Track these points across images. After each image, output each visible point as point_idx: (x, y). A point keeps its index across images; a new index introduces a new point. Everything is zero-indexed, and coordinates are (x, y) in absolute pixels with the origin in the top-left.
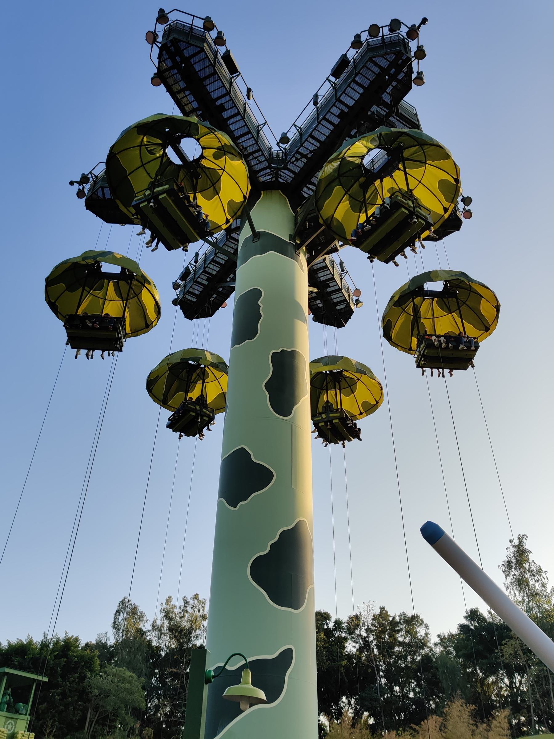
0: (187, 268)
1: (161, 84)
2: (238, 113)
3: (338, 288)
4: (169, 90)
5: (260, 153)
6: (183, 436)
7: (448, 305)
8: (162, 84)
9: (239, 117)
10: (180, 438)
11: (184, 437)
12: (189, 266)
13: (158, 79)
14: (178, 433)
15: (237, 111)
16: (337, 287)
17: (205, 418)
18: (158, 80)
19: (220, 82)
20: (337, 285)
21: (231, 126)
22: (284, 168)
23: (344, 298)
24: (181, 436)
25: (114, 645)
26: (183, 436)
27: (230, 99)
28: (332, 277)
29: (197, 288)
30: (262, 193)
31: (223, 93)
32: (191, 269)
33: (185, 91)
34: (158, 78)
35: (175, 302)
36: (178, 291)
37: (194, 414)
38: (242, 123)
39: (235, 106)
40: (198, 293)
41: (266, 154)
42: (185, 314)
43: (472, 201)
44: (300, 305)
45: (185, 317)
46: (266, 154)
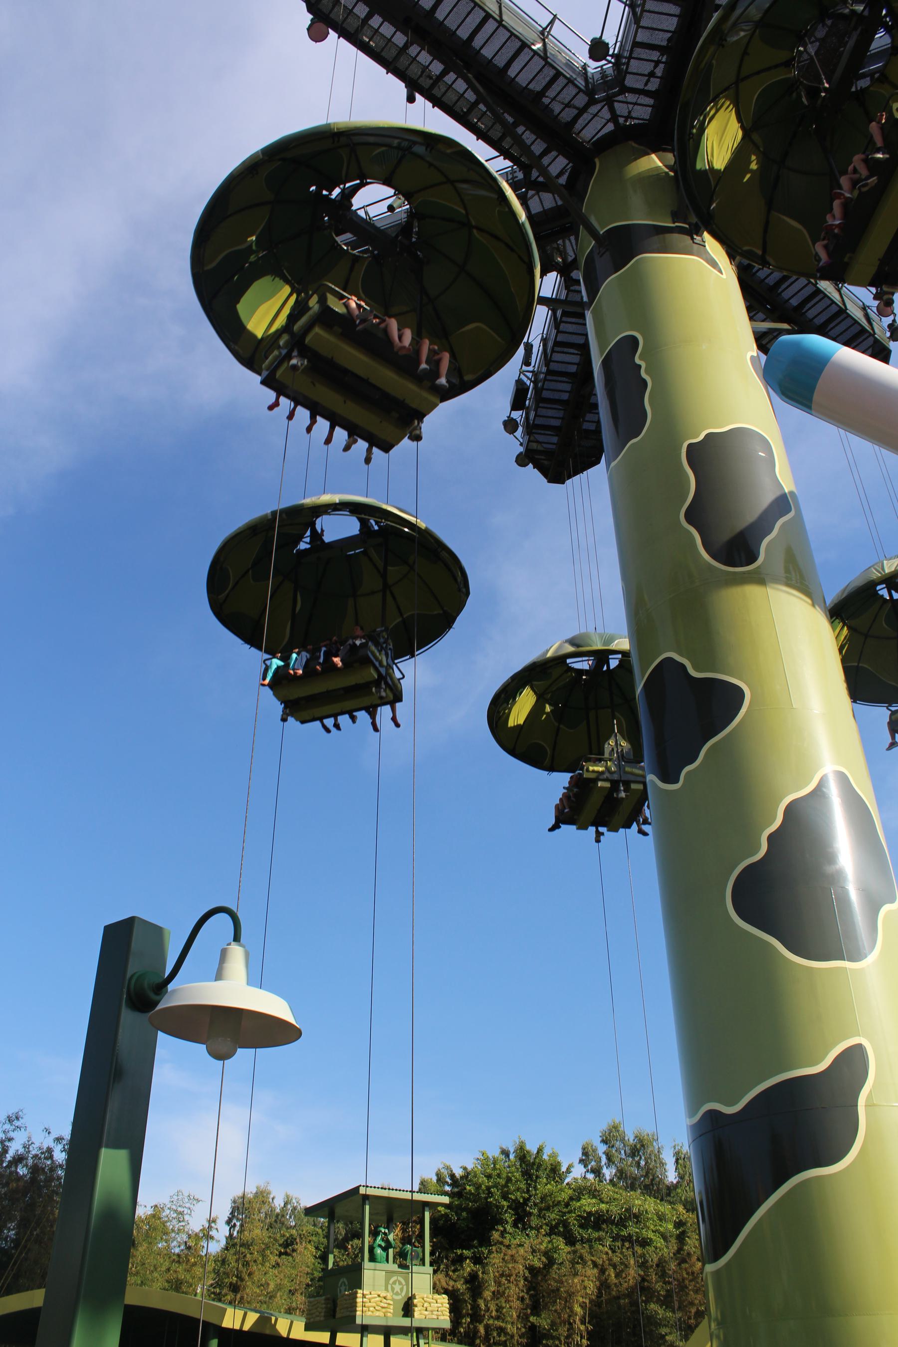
0: (519, 382)
1: (328, 33)
2: (488, 16)
3: (838, 309)
4: (344, 34)
5: (561, 81)
6: (603, 834)
7: (575, 248)
8: (330, 30)
9: (491, 25)
10: (598, 841)
11: (608, 836)
12: (522, 377)
13: (321, 24)
14: (592, 829)
15: (519, 44)
16: (834, 309)
17: (633, 786)
18: (321, 26)
19: (828, 300)
20: (833, 302)
21: (483, 52)
22: (622, 92)
23: (858, 329)
24: (599, 835)
25: (646, 1304)
26: (603, 834)
27: (577, 90)
28: (815, 289)
29: (550, 413)
30: (597, 161)
31: (481, 17)
32: (525, 379)
33: (437, 59)
34: (320, 22)
35: (522, 461)
36: (519, 432)
37: (607, 785)
38: (503, 35)
39: (512, 34)
40: (557, 423)
41: (581, 82)
42: (545, 476)
43: (525, 466)
44: (769, 942)
45: (549, 482)
46: (581, 82)
